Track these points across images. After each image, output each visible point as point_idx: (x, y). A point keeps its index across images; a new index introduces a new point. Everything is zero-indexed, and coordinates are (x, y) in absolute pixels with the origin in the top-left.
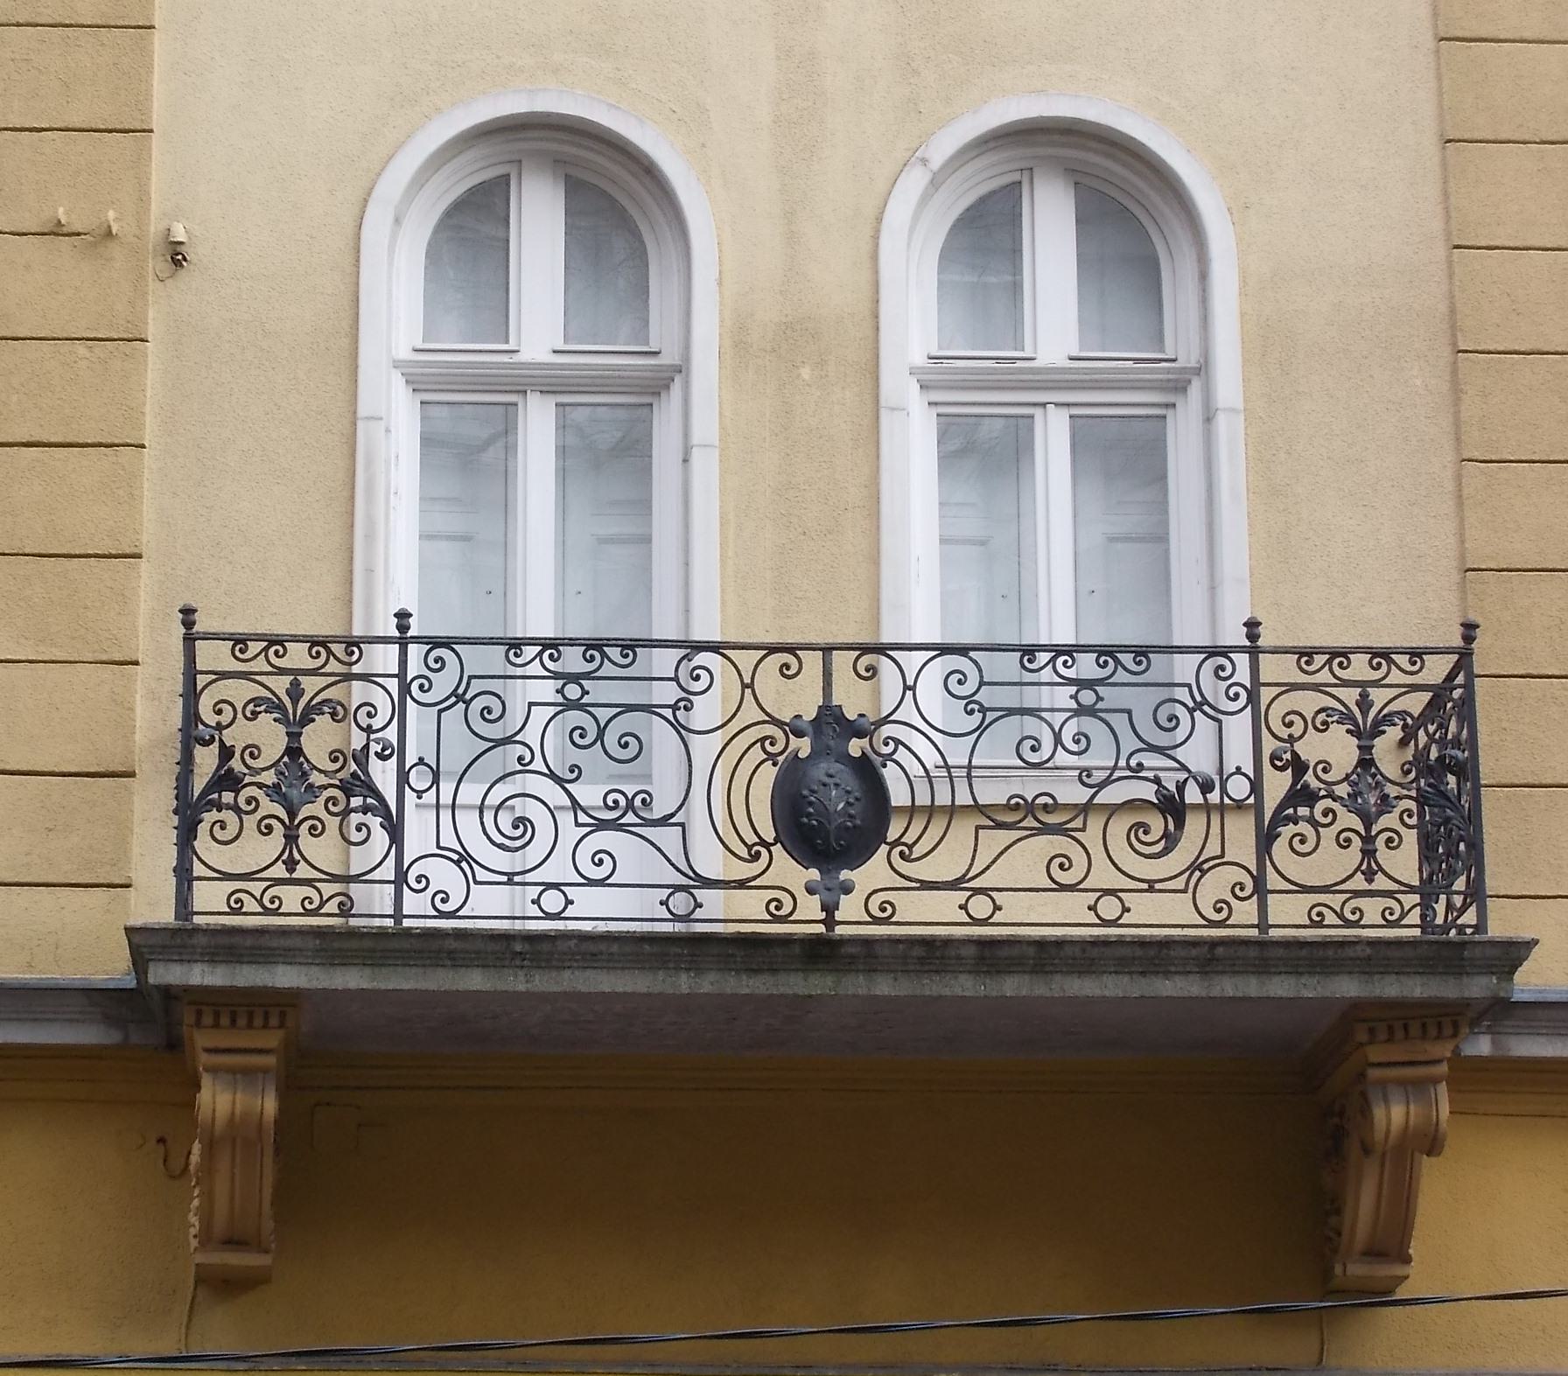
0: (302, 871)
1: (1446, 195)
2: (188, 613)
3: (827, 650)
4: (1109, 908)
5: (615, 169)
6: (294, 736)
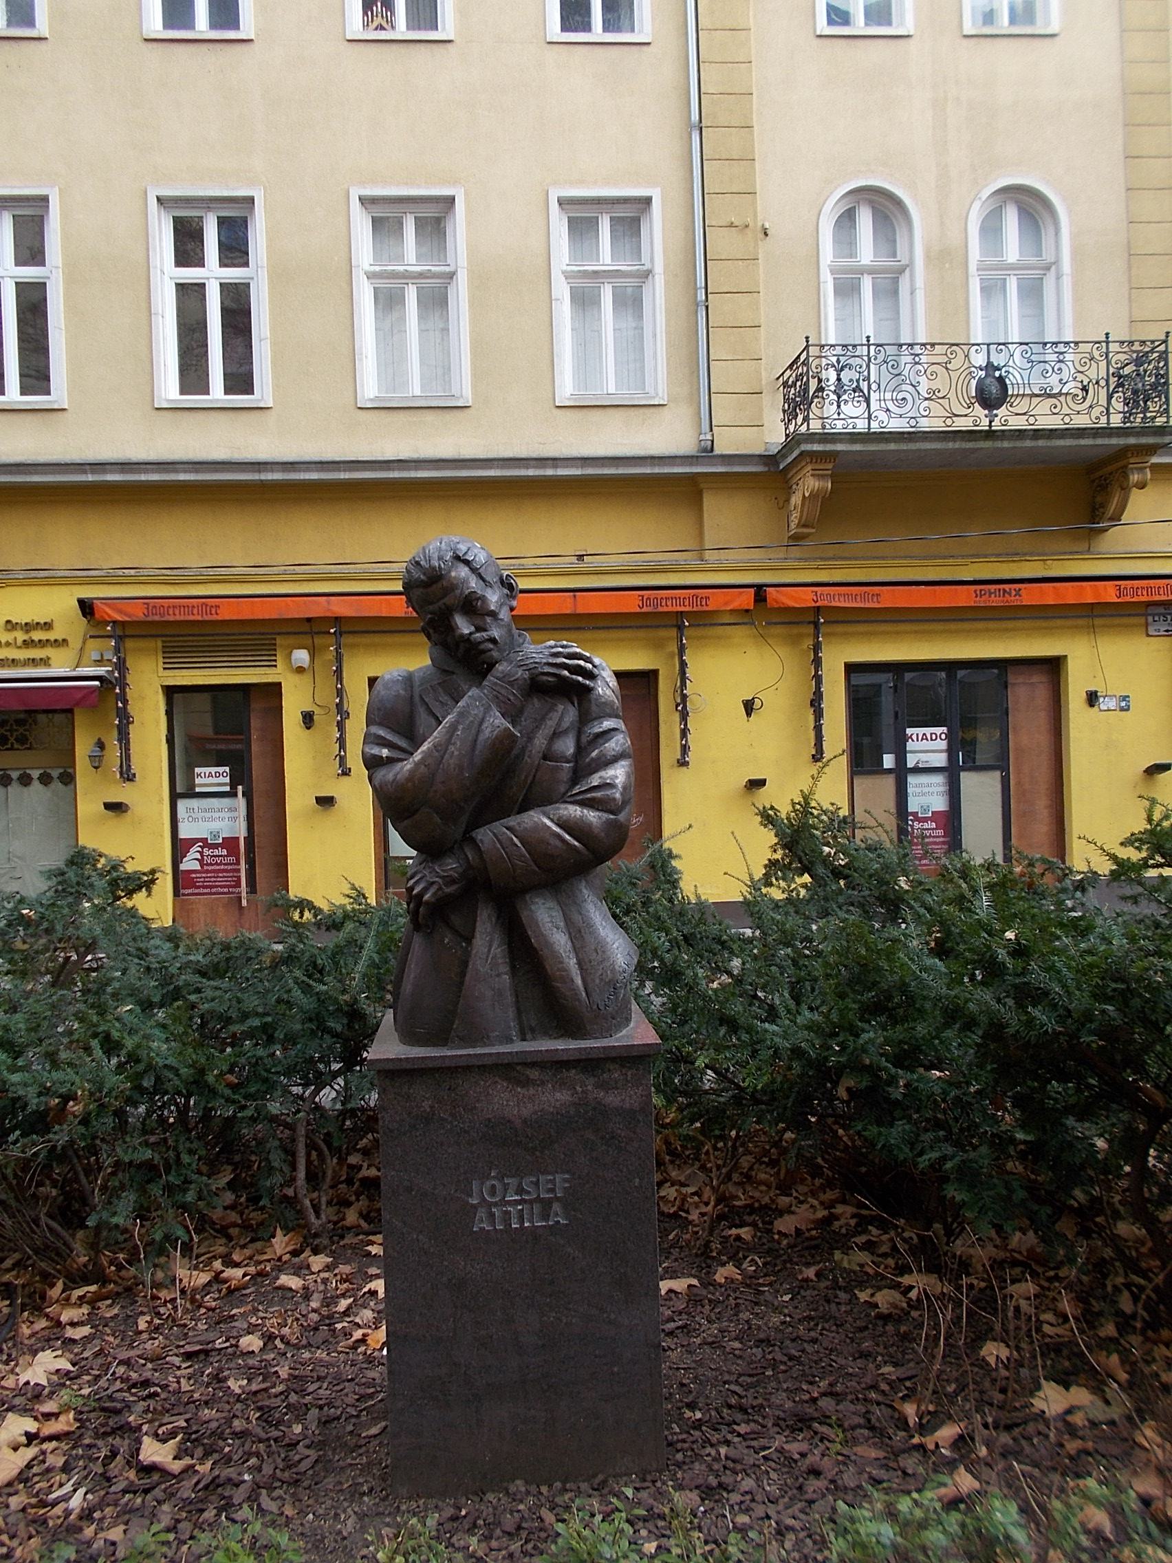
0: (842, 416)
1: (1127, 206)
2: (807, 338)
3: (988, 345)
4: (1067, 420)
5: (887, 203)
6: (838, 375)
